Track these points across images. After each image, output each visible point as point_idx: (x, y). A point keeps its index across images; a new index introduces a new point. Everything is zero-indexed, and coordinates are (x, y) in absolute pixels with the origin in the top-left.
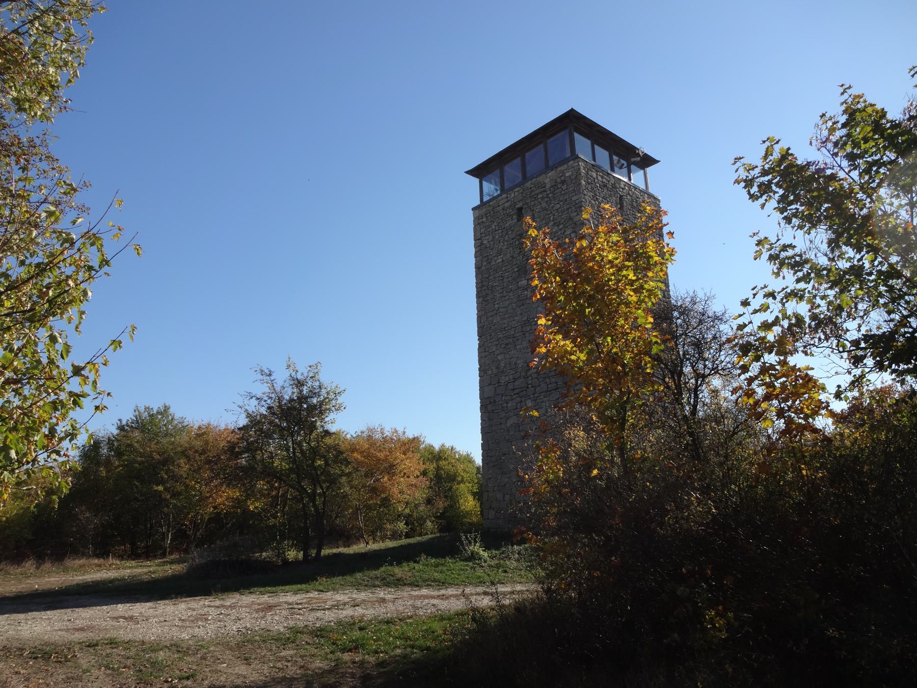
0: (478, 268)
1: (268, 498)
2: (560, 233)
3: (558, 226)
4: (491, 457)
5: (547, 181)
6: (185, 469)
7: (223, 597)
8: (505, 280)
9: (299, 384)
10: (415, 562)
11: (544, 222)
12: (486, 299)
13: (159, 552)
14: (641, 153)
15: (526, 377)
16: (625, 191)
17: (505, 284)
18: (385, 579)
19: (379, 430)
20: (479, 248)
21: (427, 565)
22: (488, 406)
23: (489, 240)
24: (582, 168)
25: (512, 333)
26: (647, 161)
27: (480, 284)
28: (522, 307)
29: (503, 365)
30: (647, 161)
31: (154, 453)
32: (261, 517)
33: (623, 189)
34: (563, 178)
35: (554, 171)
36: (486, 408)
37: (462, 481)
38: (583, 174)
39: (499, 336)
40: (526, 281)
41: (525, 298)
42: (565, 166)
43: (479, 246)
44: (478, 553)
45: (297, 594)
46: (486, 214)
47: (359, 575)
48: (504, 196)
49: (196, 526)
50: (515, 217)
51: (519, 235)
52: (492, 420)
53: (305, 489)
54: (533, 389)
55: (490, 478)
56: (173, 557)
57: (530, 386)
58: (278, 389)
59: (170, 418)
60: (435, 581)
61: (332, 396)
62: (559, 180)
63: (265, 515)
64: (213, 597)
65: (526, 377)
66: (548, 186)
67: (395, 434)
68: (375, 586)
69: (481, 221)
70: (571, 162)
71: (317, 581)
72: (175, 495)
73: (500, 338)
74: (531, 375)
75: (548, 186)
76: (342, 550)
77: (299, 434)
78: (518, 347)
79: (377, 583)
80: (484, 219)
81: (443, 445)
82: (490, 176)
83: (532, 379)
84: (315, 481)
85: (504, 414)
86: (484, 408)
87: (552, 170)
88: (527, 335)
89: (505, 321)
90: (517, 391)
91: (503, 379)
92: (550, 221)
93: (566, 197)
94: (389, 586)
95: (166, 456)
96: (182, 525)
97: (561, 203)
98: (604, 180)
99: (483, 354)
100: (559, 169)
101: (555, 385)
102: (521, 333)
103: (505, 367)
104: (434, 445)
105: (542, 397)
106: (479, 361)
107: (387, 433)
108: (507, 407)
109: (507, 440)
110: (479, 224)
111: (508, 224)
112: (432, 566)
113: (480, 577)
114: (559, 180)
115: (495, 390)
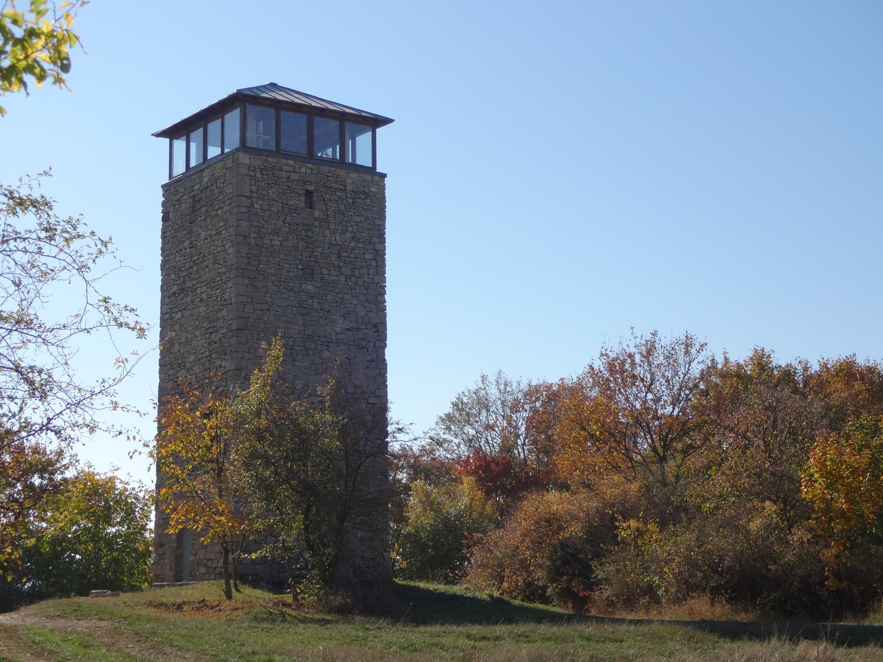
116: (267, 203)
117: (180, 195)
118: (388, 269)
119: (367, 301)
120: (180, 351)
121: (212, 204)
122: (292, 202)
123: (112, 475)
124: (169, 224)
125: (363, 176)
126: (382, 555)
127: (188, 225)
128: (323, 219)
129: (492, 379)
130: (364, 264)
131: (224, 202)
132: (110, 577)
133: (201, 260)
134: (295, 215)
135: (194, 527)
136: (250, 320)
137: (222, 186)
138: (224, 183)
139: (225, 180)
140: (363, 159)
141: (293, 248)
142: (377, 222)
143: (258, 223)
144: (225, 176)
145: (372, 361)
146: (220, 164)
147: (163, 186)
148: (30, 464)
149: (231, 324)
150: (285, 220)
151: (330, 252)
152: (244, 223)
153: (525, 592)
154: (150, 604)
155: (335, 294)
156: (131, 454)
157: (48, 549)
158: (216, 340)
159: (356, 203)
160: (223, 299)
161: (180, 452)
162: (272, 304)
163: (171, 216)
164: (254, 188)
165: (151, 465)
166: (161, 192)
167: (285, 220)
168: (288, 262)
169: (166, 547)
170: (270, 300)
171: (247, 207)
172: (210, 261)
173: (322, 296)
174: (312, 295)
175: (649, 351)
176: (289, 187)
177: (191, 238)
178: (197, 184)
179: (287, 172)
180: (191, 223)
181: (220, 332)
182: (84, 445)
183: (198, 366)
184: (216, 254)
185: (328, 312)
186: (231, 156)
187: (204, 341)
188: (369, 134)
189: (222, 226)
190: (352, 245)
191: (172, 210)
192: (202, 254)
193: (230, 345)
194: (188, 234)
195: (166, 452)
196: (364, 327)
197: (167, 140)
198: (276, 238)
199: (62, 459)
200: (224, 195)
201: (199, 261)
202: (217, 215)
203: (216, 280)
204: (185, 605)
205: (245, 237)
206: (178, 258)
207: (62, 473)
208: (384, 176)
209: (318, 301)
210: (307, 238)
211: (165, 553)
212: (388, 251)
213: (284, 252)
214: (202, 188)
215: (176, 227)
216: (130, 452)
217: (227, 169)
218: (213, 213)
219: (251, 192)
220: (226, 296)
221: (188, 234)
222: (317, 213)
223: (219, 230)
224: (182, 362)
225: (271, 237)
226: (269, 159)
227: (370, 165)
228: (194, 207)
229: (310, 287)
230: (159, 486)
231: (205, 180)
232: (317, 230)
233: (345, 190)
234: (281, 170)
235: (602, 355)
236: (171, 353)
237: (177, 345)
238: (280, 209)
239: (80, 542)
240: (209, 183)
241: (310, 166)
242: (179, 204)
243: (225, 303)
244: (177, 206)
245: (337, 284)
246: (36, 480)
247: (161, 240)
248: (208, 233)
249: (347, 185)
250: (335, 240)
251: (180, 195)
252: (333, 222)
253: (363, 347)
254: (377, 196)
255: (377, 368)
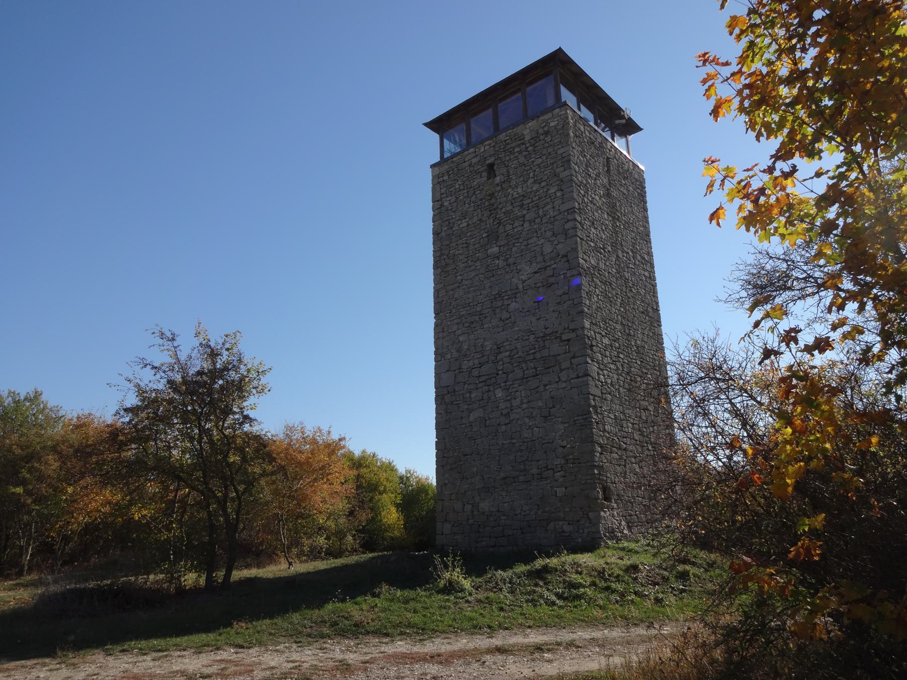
0: (436, 233)
1: (161, 503)
2: (541, 191)
3: (540, 183)
4: (448, 458)
5: (526, 132)
6: (53, 467)
7: (75, 661)
8: (471, 247)
9: (213, 354)
10: (374, 595)
11: (521, 179)
12: (446, 270)
13: (14, 570)
14: (626, 116)
15: (496, 362)
16: (611, 153)
17: (471, 252)
18: (336, 624)
19: (299, 428)
20: (439, 210)
21: (392, 600)
22: (446, 397)
23: (452, 201)
24: (570, 118)
25: (479, 309)
26: (629, 128)
27: (439, 254)
28: (492, 279)
29: (467, 347)
30: (629, 128)
31: (14, 447)
32: (150, 529)
33: (609, 150)
34: (546, 129)
35: (535, 121)
36: (443, 399)
37: (385, 491)
38: (571, 124)
39: (463, 313)
40: (498, 248)
41: (496, 268)
42: (550, 115)
43: (438, 209)
44: (458, 583)
45: (200, 653)
46: (448, 172)
47: (296, 617)
48: (472, 150)
49: (66, 539)
50: (484, 174)
51: (489, 196)
52: (451, 413)
53: (213, 492)
54: (504, 376)
55: (445, 484)
56: (28, 578)
57: (500, 372)
58: (183, 357)
59: (42, 406)
60: (409, 626)
61: (253, 375)
62: (541, 131)
63: (155, 526)
64: (59, 660)
65: (496, 362)
66: (527, 138)
67: (318, 434)
68: (322, 636)
69: (441, 179)
70: (557, 110)
71: (232, 628)
72: (38, 500)
73: (463, 315)
74: (502, 360)
75: (527, 138)
76: (253, 572)
77: (208, 420)
78: (486, 326)
79: (326, 630)
80: (446, 178)
81: (364, 452)
82: (451, 131)
83: (503, 364)
84: (228, 481)
85: (466, 407)
86: (440, 399)
87: (533, 120)
88: (498, 311)
89: (470, 296)
90: (484, 378)
91: (466, 365)
92: (529, 178)
93: (550, 150)
94: (344, 636)
95: (30, 450)
96: (48, 537)
97: (544, 157)
98: (592, 137)
99: (441, 335)
100: (541, 118)
101: (534, 370)
102: (489, 310)
103: (468, 349)
104: (355, 452)
105: (516, 385)
106: (435, 343)
107: (308, 433)
108: (470, 397)
109: (470, 438)
110: (439, 183)
111: (475, 183)
112: (399, 601)
113: (471, 619)
114: (541, 131)
115: (455, 377)
174: (497, 255)
195: (802, 420)
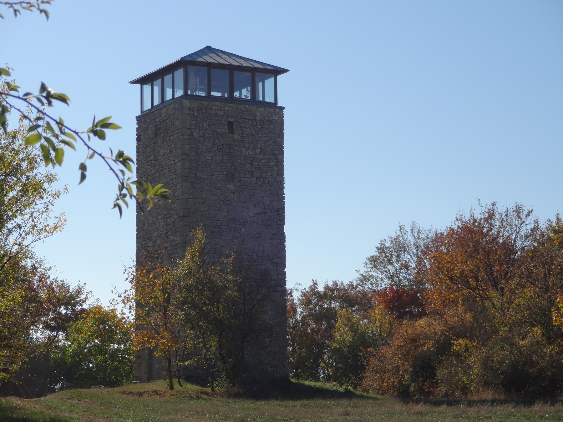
116: (202, 132)
117: (147, 124)
118: (285, 171)
119: (271, 194)
120: (148, 229)
121: (167, 132)
122: (219, 130)
123: (114, 308)
124: (141, 143)
125: (268, 109)
126: (283, 364)
127: (153, 145)
128: (240, 140)
129: (408, 228)
130: (269, 169)
131: (174, 132)
132: (113, 379)
133: (161, 169)
134: (221, 138)
135: (149, 346)
136: (192, 210)
137: (173, 121)
138: (174, 119)
139: (175, 117)
140: (270, 99)
141: (220, 161)
142: (278, 140)
143: (196, 145)
144: (175, 114)
145: (275, 234)
146: (172, 106)
147: (137, 117)
148: (58, 298)
149: (179, 213)
150: (214, 142)
151: (245, 162)
152: (187, 146)
153: (399, 389)
154: (124, 393)
155: (249, 190)
156: (111, 301)
157: (70, 360)
158: (170, 223)
159: (264, 128)
160: (174, 196)
161: (141, 300)
162: (206, 199)
163: (142, 138)
164: (193, 122)
165: (123, 308)
166: (135, 121)
167: (214, 142)
168: (217, 170)
169: (142, 358)
170: (204, 196)
171: (189, 135)
172: (167, 170)
173: (240, 192)
175: (491, 215)
176: (217, 121)
177: (154, 153)
178: (158, 118)
179: (215, 110)
180: (154, 144)
181: (173, 217)
182: (131, 258)
183: (160, 239)
184: (170, 166)
185: (244, 202)
186: (178, 101)
187: (163, 223)
188: (273, 79)
189: (173, 147)
190: (260, 157)
191: (142, 134)
192: (161, 165)
193: (179, 227)
194: (153, 151)
196: (269, 211)
197: (140, 85)
198: (208, 154)
199: (81, 295)
200: (174, 127)
201: (159, 170)
202: (170, 140)
203: (170, 183)
204: (145, 393)
205: (188, 155)
206: (146, 167)
207: (81, 305)
208: (283, 108)
209: (237, 195)
210: (230, 154)
211: (141, 363)
212: (285, 160)
213: (214, 164)
214: (161, 121)
215: (145, 145)
216: (110, 300)
217: (176, 109)
218: (168, 138)
219: (191, 125)
220: (176, 194)
221: (153, 151)
222: (236, 137)
223: (171, 150)
224: (150, 236)
225: (205, 154)
226: (203, 102)
227: (273, 102)
228: (156, 133)
229: (231, 187)
230: (136, 319)
231: (163, 115)
232: (236, 148)
233: (255, 120)
234: (212, 109)
235: (457, 220)
236: (144, 230)
237: (147, 225)
238: (211, 135)
239: (92, 355)
240: (165, 118)
241: (231, 105)
242: (147, 130)
243: (175, 199)
244: (146, 132)
245: (250, 183)
246: (63, 311)
247: (136, 154)
248: (165, 151)
249: (257, 116)
250: (249, 154)
251: (147, 124)
252: (247, 142)
253: (269, 225)
254: (278, 122)
255: (278, 239)
